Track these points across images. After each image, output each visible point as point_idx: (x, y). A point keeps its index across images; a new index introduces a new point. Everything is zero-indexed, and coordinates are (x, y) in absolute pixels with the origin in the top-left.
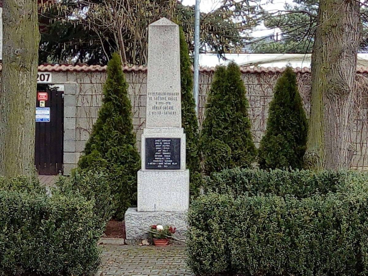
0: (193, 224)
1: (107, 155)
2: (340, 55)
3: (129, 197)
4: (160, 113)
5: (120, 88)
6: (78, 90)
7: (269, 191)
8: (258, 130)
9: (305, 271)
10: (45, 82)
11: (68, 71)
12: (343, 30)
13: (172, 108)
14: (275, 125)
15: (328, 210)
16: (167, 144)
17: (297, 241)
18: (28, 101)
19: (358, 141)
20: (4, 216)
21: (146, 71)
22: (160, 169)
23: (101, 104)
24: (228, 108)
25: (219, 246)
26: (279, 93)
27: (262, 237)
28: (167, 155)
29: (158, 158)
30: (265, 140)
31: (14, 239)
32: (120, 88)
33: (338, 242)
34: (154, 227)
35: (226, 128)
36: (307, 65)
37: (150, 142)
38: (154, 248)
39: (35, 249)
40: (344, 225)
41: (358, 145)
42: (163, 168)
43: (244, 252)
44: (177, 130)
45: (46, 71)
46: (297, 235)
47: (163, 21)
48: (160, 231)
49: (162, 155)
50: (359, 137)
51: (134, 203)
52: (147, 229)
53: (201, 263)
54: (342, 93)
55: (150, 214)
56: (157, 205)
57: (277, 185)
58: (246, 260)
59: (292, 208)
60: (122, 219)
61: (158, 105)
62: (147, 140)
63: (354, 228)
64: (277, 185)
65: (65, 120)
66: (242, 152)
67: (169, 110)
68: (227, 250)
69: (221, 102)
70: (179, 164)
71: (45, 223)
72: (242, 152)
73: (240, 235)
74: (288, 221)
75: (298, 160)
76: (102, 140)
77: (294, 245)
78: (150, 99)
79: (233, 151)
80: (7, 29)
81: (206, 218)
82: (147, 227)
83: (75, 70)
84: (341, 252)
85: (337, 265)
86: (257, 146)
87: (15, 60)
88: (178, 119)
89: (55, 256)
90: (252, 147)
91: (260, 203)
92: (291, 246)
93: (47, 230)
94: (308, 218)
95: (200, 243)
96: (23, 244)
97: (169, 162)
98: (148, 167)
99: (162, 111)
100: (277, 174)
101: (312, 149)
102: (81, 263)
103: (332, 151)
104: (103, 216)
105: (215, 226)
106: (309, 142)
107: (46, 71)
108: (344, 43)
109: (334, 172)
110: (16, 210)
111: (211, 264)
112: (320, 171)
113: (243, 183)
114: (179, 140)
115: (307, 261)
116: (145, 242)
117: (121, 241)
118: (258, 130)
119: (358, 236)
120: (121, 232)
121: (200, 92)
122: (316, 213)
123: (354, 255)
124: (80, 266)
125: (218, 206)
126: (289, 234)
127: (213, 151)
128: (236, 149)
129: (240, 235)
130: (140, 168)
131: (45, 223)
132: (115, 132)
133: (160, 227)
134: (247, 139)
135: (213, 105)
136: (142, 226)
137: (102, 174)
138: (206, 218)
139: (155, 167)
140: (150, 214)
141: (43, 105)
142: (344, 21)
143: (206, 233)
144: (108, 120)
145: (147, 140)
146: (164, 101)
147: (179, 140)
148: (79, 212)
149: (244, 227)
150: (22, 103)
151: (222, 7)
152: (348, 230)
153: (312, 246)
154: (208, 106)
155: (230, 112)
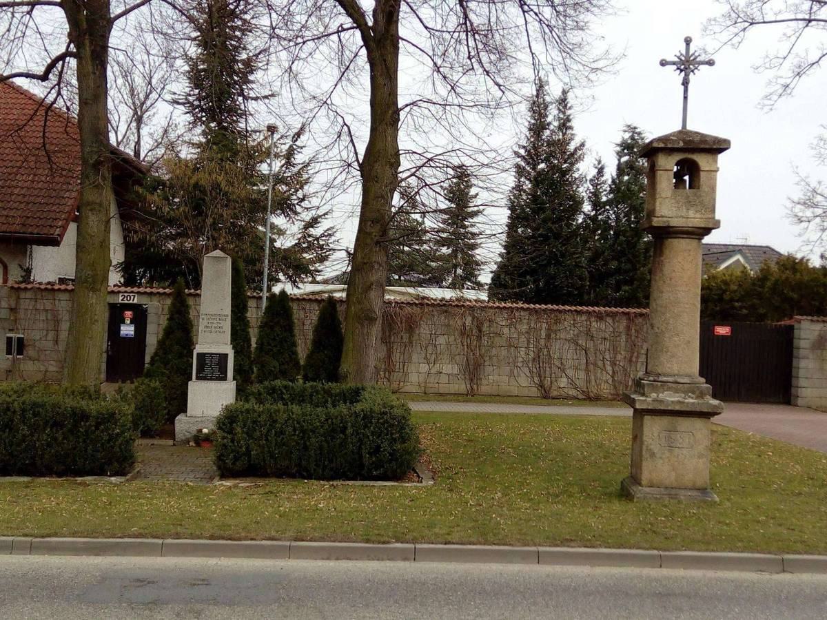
0: (220, 428)
1: (168, 367)
2: (369, 288)
3: (180, 403)
4: (211, 332)
5: (183, 309)
6: (161, 309)
7: (303, 401)
8: (303, 350)
9: (315, 470)
10: (131, 302)
11: (151, 293)
12: (373, 267)
13: (222, 327)
14: (318, 344)
15: (336, 417)
16: (216, 359)
17: (308, 443)
18: (96, 317)
19: (401, 360)
20: (48, 418)
21: (199, 295)
22: (208, 380)
23: (166, 322)
24: (277, 329)
25: (241, 447)
26: (322, 318)
27: (279, 440)
28: (216, 368)
29: (207, 370)
30: (309, 357)
31: (56, 439)
32: (183, 309)
33: (343, 444)
34: (200, 431)
35: (276, 346)
36: (344, 295)
37: (201, 356)
38: (198, 449)
39: (74, 449)
40: (350, 431)
41: (401, 364)
42: (211, 379)
43: (262, 452)
44: (226, 346)
45: (132, 292)
46: (309, 438)
47: (218, 253)
48: (205, 434)
49: (213, 368)
50: (402, 357)
51: (185, 411)
52: (194, 433)
53: (225, 463)
54: (372, 320)
55: (197, 419)
56: (205, 411)
57: (311, 395)
58: (264, 461)
59: (306, 415)
60: (173, 423)
61: (210, 325)
62: (198, 354)
63: (358, 434)
64: (311, 395)
65: (148, 335)
66: (289, 367)
67: (220, 330)
68: (248, 450)
69: (271, 324)
70: (226, 375)
71: (85, 425)
72: (289, 367)
73: (260, 438)
74: (302, 426)
75: (334, 376)
76: (165, 354)
77: (306, 448)
78: (203, 319)
79: (280, 365)
80: (80, 254)
81: (231, 423)
82: (194, 429)
83: (158, 293)
84: (346, 454)
85: (342, 464)
86: (302, 362)
87: (86, 282)
88: (228, 336)
89: (92, 456)
90: (298, 363)
91: (278, 411)
92: (303, 448)
93: (86, 431)
94: (318, 424)
95: (224, 445)
96: (64, 443)
97: (217, 374)
98: (198, 378)
99: (213, 330)
100: (311, 386)
101: (345, 367)
102: (117, 461)
103: (360, 371)
104: (156, 420)
105: (239, 430)
106: (342, 360)
107: (132, 292)
108: (374, 277)
109: (359, 385)
110: (58, 413)
111: (233, 464)
112: (351, 384)
113: (282, 393)
114: (226, 355)
115: (316, 461)
116: (192, 443)
117: (171, 442)
118: (303, 350)
119: (360, 440)
120: (171, 434)
121: (255, 314)
122: (327, 420)
123: (357, 456)
124: (116, 464)
125: (242, 412)
126: (303, 438)
127: (263, 366)
128: (283, 364)
129: (260, 438)
130: (191, 380)
131: (85, 425)
132: (177, 347)
133: (205, 431)
134: (294, 356)
135: (265, 326)
136: (190, 430)
137: (158, 383)
138: (231, 423)
139: (204, 378)
140: (197, 419)
141: (129, 322)
142: (374, 260)
143: (229, 437)
144: (171, 336)
145: (198, 354)
146: (215, 321)
147: (226, 355)
148: (117, 416)
149: (264, 431)
150: (91, 319)
151: (296, 244)
152: (352, 435)
153: (321, 448)
154: (260, 327)
155: (279, 333)
